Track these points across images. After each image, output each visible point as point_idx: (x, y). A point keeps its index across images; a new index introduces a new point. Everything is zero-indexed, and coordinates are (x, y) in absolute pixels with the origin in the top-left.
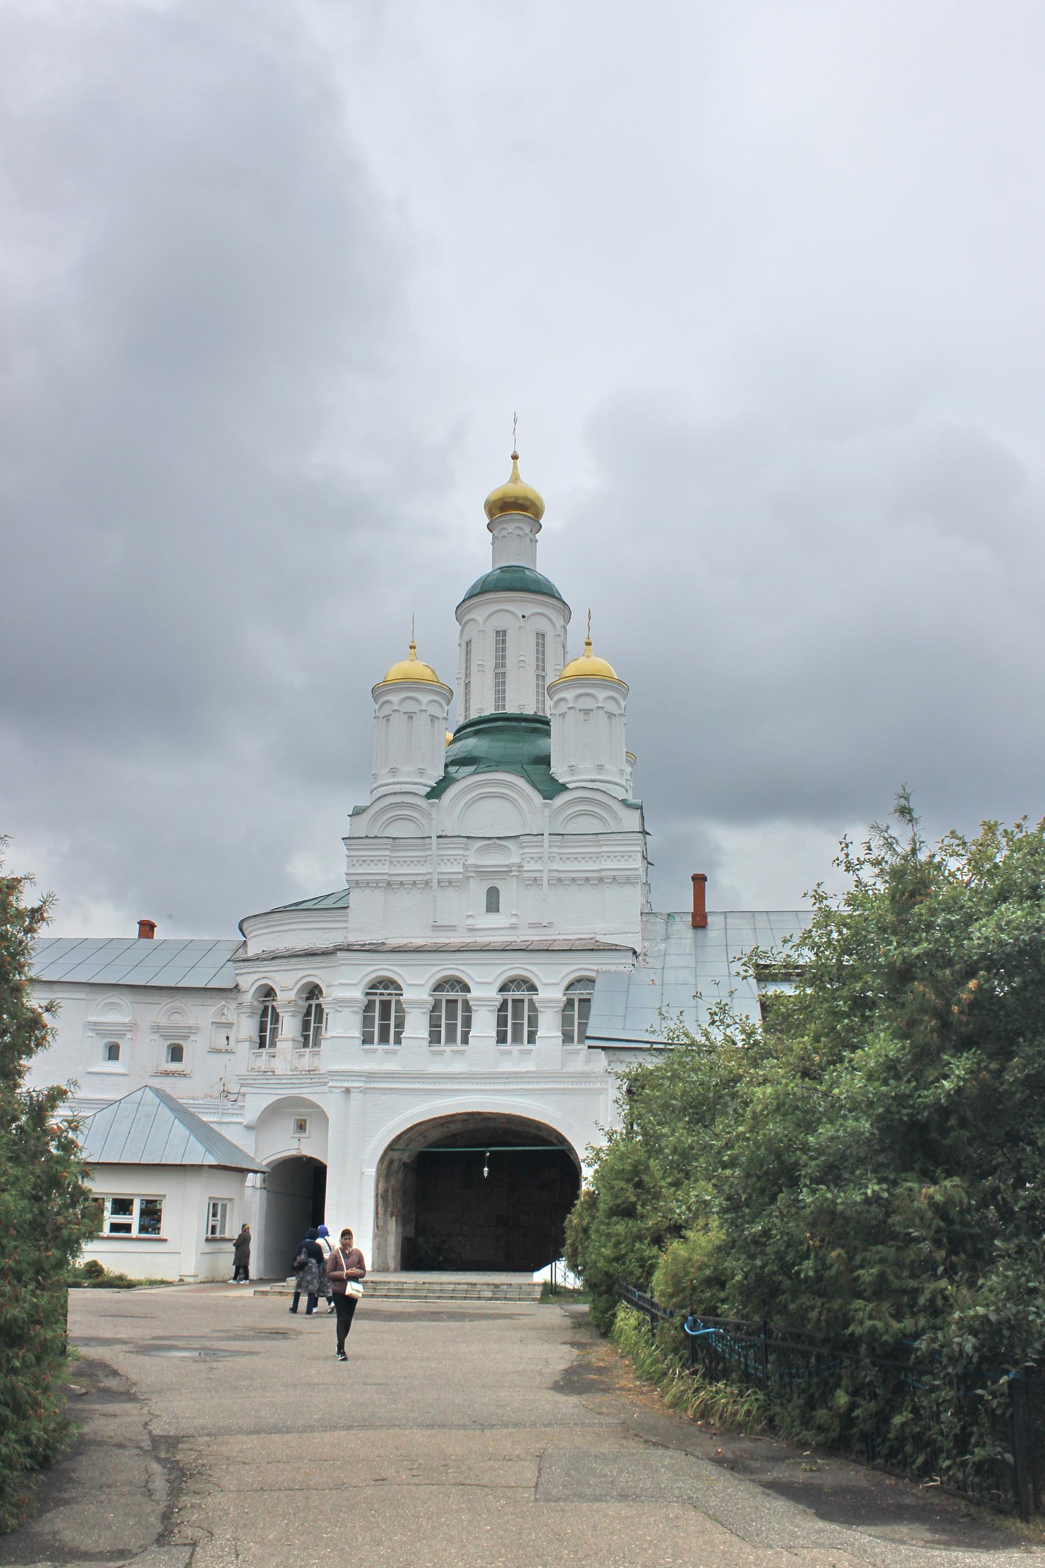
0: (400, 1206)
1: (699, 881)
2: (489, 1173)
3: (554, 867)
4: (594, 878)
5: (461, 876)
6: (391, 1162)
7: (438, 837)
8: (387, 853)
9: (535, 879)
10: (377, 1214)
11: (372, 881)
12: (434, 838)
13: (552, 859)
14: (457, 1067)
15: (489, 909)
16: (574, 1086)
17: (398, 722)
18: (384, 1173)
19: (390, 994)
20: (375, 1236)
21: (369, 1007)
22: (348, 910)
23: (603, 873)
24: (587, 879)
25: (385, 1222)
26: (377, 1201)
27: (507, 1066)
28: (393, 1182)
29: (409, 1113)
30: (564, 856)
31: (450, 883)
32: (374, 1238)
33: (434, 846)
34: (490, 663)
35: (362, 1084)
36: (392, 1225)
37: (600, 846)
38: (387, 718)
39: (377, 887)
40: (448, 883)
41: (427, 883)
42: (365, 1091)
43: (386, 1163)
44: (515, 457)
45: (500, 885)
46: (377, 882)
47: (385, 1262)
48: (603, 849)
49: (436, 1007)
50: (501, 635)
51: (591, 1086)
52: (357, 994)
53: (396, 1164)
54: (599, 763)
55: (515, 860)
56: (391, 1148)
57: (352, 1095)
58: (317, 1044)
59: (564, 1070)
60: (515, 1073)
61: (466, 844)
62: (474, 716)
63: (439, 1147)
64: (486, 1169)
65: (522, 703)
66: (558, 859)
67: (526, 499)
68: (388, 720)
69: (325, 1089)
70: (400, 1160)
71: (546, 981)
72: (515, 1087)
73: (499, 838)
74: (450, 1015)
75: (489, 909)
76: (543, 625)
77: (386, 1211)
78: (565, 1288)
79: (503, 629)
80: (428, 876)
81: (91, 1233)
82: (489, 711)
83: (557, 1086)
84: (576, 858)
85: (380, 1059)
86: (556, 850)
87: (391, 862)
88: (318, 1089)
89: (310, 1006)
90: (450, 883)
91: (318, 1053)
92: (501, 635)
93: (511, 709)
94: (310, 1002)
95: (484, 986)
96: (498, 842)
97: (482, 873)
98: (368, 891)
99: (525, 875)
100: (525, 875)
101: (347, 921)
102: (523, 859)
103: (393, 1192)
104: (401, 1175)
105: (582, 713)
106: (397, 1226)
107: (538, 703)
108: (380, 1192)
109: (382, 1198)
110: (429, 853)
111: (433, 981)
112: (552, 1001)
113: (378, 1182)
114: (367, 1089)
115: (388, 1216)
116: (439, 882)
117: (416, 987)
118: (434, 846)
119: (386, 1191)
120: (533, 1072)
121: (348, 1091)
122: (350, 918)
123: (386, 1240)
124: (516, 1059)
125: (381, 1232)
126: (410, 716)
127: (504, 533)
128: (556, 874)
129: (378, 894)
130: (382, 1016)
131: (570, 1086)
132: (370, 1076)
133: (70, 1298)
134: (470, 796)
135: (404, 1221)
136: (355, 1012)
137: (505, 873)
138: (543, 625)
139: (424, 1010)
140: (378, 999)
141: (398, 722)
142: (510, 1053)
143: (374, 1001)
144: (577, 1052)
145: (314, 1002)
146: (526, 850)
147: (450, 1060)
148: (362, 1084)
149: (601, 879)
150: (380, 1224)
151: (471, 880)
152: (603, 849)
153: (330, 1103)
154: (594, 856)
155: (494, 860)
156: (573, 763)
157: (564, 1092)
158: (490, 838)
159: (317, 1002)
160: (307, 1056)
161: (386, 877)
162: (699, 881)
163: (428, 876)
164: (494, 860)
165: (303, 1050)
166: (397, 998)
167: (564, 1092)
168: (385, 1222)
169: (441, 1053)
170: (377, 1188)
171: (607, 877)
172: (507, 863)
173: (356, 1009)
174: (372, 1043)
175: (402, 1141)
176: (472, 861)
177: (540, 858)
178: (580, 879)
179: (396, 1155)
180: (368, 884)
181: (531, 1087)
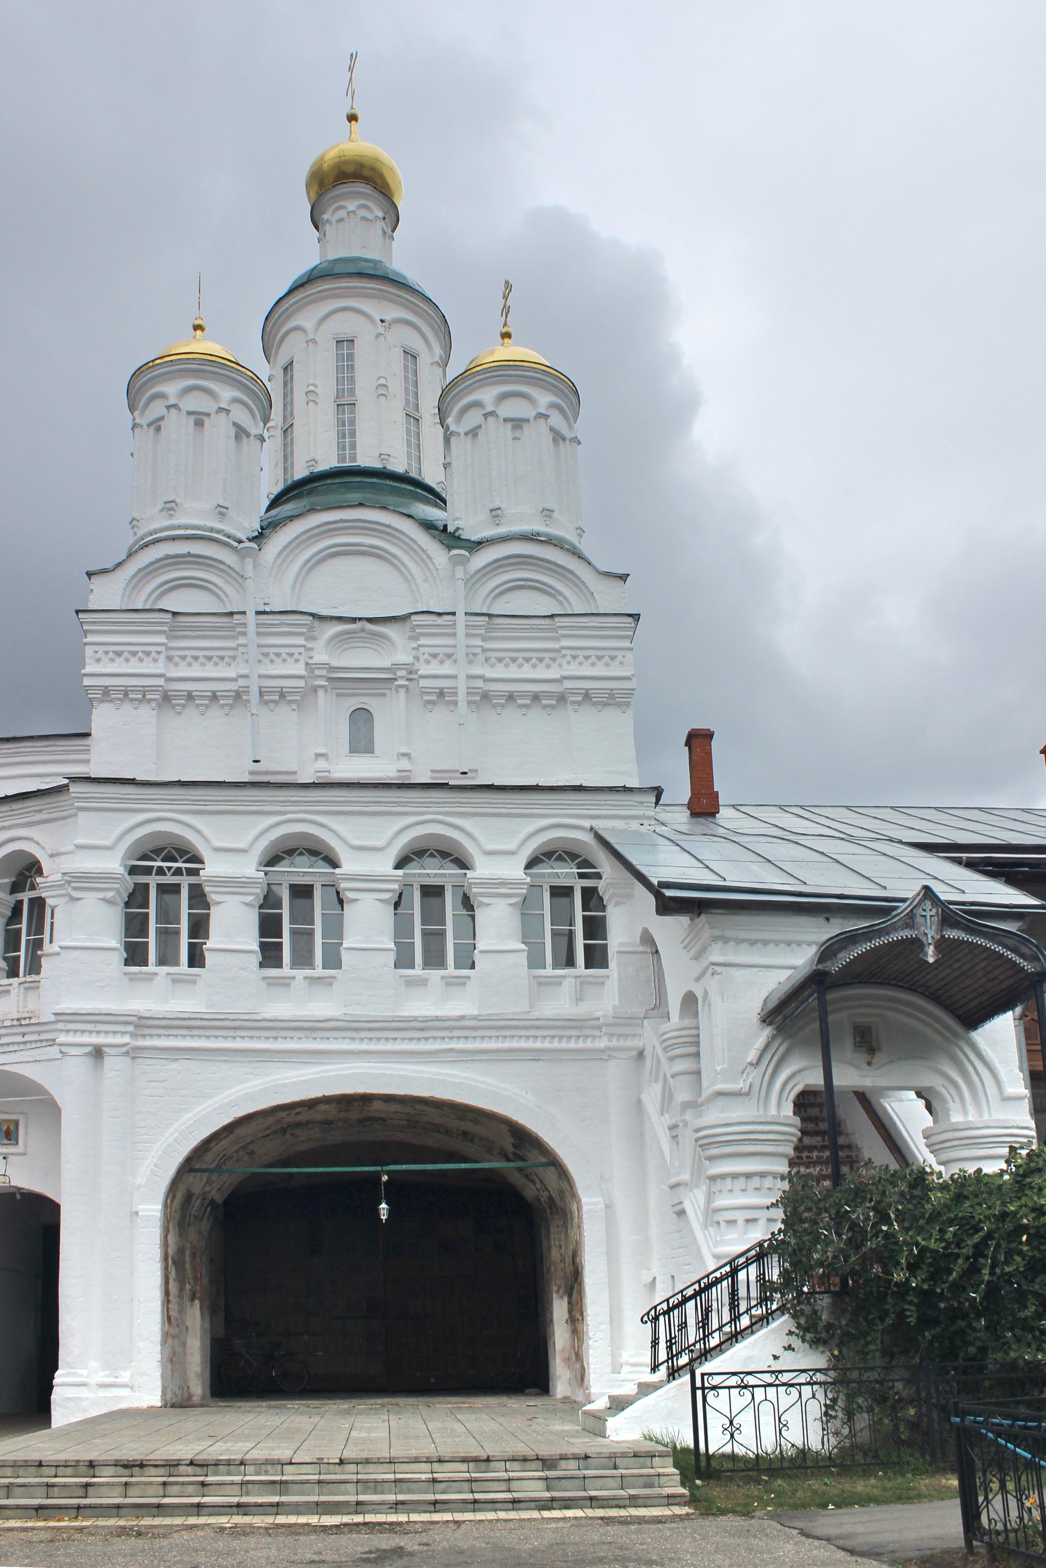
0: (205, 1281)
1: (699, 741)
2: (390, 1212)
3: (478, 671)
4: (549, 695)
5: (301, 683)
6: (189, 1197)
7: (258, 613)
8: (162, 639)
9: (441, 694)
10: (167, 1293)
11: (135, 689)
12: (251, 616)
13: (471, 658)
14: (322, 1007)
15: (354, 749)
16: (556, 1045)
17: (178, 427)
18: (177, 1216)
19: (178, 872)
20: (165, 1336)
21: (137, 897)
22: (89, 741)
23: (568, 684)
24: (536, 697)
25: (181, 1311)
26: (166, 1268)
27: (422, 1005)
28: (192, 1235)
29: (225, 1096)
30: (494, 655)
31: (282, 695)
32: (164, 1342)
33: (252, 629)
34: (327, 390)
35: (126, 1039)
36: (195, 1317)
37: (557, 639)
38: (156, 425)
39: (144, 700)
40: (277, 697)
41: (238, 696)
42: (133, 1053)
43: (180, 1195)
44: (352, 118)
45: (372, 704)
46: (144, 691)
47: (184, 1387)
48: (565, 643)
49: (270, 900)
50: (345, 343)
51: (589, 1044)
52: (114, 864)
53: (197, 1203)
54: (546, 506)
55: (403, 657)
56: (189, 1166)
57: (107, 1060)
58: (34, 967)
59: (536, 1014)
60: (437, 1019)
61: (311, 629)
62: (300, 473)
63: (275, 1167)
64: (384, 1205)
65: (385, 451)
66: (481, 658)
67: (373, 169)
68: (158, 429)
69: (54, 1051)
70: (204, 1195)
71: (490, 847)
72: (438, 1046)
73: (370, 620)
74: (292, 920)
75: (354, 749)
76: (415, 343)
77: (181, 1289)
78: (733, 1457)
79: (348, 336)
80: (242, 682)
81: (748, 1513)
82: (328, 462)
83: (523, 1044)
84: (514, 660)
85: (161, 993)
86: (478, 642)
87: (169, 658)
88: (36, 1054)
89: (20, 903)
90: (282, 695)
91: (35, 986)
92: (345, 343)
93: (366, 460)
94: (20, 896)
95: (367, 849)
96: (369, 626)
97: (341, 682)
98: (127, 708)
99: (424, 683)
100: (424, 683)
101: (87, 761)
102: (417, 658)
103: (193, 1256)
104: (205, 1225)
105: (509, 425)
106: (202, 1319)
107: (409, 457)
108: (171, 1252)
109: (176, 1264)
110: (241, 640)
111: (264, 843)
112: (503, 883)
113: (166, 1231)
114: (136, 1049)
115: (186, 1298)
116: (261, 693)
117: (232, 853)
118: (252, 629)
119: (181, 1251)
120: (474, 1018)
121: (98, 1053)
122: (93, 757)
123: (184, 1345)
124: (433, 998)
125: (172, 1331)
126: (199, 420)
127: (342, 214)
128: (480, 683)
129: (147, 714)
130: (161, 910)
131: (547, 1045)
132: (142, 1024)
133: (158, 1393)
134: (314, 549)
135: (212, 1310)
136: (108, 901)
137: (381, 683)
138: (415, 343)
139: (249, 899)
140: (153, 881)
141: (178, 427)
142: (423, 982)
143: (147, 886)
144: (557, 982)
145: (25, 896)
146: (423, 641)
147: (297, 997)
148: (126, 1039)
149: (562, 699)
150: (174, 1314)
151: (321, 693)
152: (565, 643)
153: (63, 1078)
154: (546, 655)
155: (360, 659)
156: (497, 504)
157: (536, 1055)
158: (354, 620)
159: (33, 894)
160: (14, 993)
161: (161, 682)
162: (699, 741)
163: (242, 682)
164: (360, 659)
165: (6, 981)
166: (193, 880)
167: (536, 1055)
168: (181, 1311)
169: (285, 982)
170: (165, 1244)
171: (573, 692)
172: (387, 664)
173: (110, 895)
174: (145, 963)
175: (209, 1156)
176: (321, 656)
177: (449, 656)
178: (523, 695)
179: (197, 1183)
180: (126, 694)
181: (470, 1045)
